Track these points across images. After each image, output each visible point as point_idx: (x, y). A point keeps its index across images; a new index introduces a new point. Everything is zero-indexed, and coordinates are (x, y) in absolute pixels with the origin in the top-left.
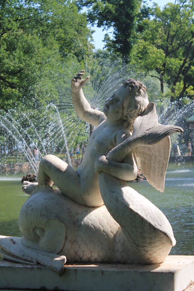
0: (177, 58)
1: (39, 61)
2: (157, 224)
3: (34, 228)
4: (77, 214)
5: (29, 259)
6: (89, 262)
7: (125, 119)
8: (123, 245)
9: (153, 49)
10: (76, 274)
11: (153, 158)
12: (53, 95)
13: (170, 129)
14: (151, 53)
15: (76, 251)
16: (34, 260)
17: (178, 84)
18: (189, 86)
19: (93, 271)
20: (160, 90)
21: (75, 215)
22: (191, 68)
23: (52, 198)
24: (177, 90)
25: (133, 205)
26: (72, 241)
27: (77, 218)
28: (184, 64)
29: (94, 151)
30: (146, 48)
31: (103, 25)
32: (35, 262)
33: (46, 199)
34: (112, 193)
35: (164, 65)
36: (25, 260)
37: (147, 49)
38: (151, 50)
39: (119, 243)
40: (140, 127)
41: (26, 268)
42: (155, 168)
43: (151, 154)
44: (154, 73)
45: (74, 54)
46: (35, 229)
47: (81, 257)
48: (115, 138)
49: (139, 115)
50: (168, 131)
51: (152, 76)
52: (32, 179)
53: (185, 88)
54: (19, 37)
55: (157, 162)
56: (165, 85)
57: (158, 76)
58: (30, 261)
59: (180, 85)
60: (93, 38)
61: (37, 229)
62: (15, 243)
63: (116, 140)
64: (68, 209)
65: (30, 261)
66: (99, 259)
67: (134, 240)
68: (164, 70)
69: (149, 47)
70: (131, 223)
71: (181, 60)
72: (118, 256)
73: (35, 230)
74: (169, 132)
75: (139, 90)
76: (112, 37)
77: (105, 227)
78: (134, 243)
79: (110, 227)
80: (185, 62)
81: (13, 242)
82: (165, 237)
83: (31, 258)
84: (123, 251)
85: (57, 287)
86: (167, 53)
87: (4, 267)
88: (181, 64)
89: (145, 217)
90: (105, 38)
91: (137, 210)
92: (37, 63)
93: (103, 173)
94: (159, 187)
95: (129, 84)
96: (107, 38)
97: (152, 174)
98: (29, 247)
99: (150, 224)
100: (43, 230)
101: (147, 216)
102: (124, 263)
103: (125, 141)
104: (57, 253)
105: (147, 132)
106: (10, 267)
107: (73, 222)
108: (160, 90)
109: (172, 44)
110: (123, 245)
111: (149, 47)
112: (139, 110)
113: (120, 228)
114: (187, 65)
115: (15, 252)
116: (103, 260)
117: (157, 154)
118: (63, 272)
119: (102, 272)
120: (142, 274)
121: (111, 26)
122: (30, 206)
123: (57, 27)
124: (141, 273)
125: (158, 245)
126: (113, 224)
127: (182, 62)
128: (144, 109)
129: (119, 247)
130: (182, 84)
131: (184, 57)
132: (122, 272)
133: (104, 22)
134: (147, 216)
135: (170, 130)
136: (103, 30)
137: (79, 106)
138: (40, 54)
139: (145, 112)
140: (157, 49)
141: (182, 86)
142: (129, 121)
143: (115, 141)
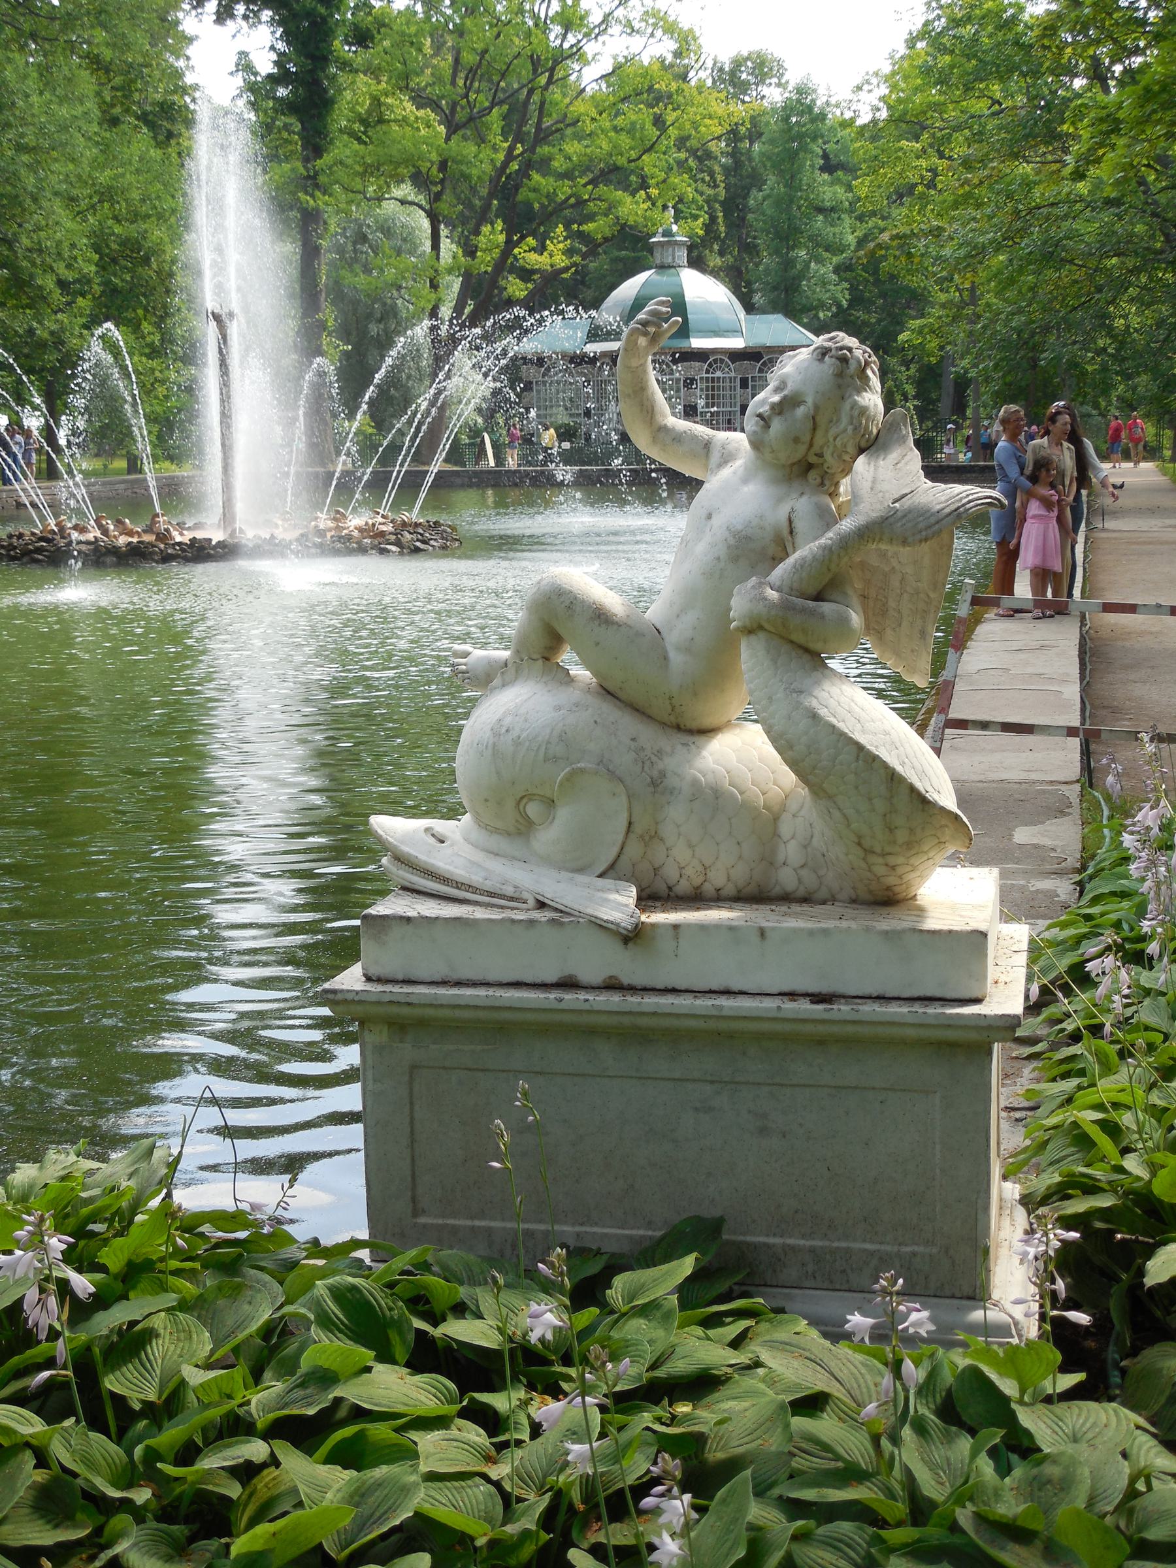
0: (484, 142)
1: (30, 140)
2: (930, 789)
3: (522, 798)
4: (659, 753)
5: (509, 890)
6: (696, 899)
7: (812, 459)
8: (805, 847)
9: (404, 109)
10: (677, 938)
11: (895, 582)
12: (80, 260)
13: (971, 498)
14: (396, 121)
15: (656, 866)
16: (525, 895)
17: (486, 229)
18: (523, 238)
19: (731, 928)
20: (429, 250)
21: (654, 759)
22: (529, 177)
23: (577, 705)
24: (484, 251)
25: (863, 731)
26: (647, 838)
27: (661, 766)
28: (505, 164)
29: (718, 559)
30: (380, 104)
31: (232, 16)
32: (532, 902)
33: (558, 708)
34: (795, 695)
35: (443, 166)
36: (492, 894)
37: (383, 108)
38: (399, 113)
39: (793, 842)
40: (872, 489)
41: (513, 921)
42: (899, 612)
43: (887, 569)
44: (405, 190)
45: (138, 118)
46: (525, 801)
47: (671, 883)
48: (790, 521)
49: (861, 451)
50: (963, 505)
51: (403, 202)
52: (31, 547)
53: (510, 244)
54: (646, 226)
55: (905, 595)
56: (444, 231)
57: (421, 199)
58: (512, 899)
59: (493, 235)
60: (191, 63)
61: (530, 800)
62: (443, 842)
63: (795, 530)
64: (633, 740)
65: (512, 899)
66: (730, 890)
67: (860, 837)
68: (442, 181)
69: (389, 101)
70: (857, 788)
71: (495, 149)
72: (787, 879)
73: (521, 807)
74: (968, 506)
75: (864, 370)
76: (265, 65)
77: (747, 794)
78: (859, 844)
79: (763, 794)
80: (510, 157)
81: (433, 835)
82: (950, 825)
83: (516, 887)
84: (802, 866)
85: (611, 977)
86: (453, 128)
87: (437, 918)
88: (498, 164)
89: (899, 769)
90: (237, 65)
91: (876, 747)
92: (20, 148)
93: (761, 635)
94: (913, 670)
95: (833, 352)
96: (244, 65)
97: (889, 631)
98: (497, 854)
99: (912, 789)
100: (550, 803)
101: (903, 764)
102: (805, 900)
103: (830, 534)
104: (598, 873)
105: (896, 505)
106: (457, 920)
107: (649, 780)
108: (427, 246)
109: (466, 96)
110: (805, 847)
111: (389, 101)
112: (863, 435)
113: (808, 799)
114: (514, 166)
115: (451, 868)
116: (739, 891)
117: (909, 570)
118: (633, 936)
119: (762, 933)
120: (889, 936)
121: (260, 22)
122: (507, 731)
123: (847, 221)
124: (886, 933)
125: (926, 849)
126: (771, 785)
127: (501, 156)
128: (875, 431)
129: (791, 852)
130: (501, 232)
131: (506, 140)
132: (825, 932)
133: (237, 7)
134: (903, 764)
135: (970, 502)
136: (234, 36)
137: (642, 411)
138: (33, 115)
139: (880, 440)
140: (417, 109)
141: (502, 238)
142: (826, 466)
143: (791, 532)
